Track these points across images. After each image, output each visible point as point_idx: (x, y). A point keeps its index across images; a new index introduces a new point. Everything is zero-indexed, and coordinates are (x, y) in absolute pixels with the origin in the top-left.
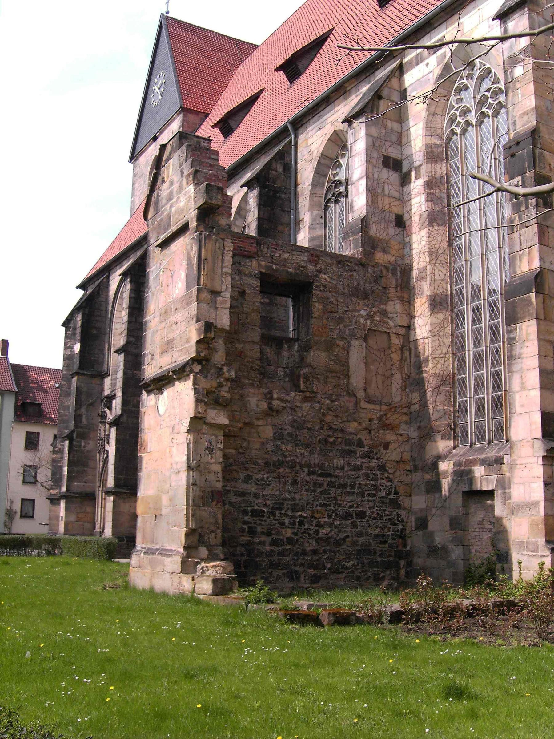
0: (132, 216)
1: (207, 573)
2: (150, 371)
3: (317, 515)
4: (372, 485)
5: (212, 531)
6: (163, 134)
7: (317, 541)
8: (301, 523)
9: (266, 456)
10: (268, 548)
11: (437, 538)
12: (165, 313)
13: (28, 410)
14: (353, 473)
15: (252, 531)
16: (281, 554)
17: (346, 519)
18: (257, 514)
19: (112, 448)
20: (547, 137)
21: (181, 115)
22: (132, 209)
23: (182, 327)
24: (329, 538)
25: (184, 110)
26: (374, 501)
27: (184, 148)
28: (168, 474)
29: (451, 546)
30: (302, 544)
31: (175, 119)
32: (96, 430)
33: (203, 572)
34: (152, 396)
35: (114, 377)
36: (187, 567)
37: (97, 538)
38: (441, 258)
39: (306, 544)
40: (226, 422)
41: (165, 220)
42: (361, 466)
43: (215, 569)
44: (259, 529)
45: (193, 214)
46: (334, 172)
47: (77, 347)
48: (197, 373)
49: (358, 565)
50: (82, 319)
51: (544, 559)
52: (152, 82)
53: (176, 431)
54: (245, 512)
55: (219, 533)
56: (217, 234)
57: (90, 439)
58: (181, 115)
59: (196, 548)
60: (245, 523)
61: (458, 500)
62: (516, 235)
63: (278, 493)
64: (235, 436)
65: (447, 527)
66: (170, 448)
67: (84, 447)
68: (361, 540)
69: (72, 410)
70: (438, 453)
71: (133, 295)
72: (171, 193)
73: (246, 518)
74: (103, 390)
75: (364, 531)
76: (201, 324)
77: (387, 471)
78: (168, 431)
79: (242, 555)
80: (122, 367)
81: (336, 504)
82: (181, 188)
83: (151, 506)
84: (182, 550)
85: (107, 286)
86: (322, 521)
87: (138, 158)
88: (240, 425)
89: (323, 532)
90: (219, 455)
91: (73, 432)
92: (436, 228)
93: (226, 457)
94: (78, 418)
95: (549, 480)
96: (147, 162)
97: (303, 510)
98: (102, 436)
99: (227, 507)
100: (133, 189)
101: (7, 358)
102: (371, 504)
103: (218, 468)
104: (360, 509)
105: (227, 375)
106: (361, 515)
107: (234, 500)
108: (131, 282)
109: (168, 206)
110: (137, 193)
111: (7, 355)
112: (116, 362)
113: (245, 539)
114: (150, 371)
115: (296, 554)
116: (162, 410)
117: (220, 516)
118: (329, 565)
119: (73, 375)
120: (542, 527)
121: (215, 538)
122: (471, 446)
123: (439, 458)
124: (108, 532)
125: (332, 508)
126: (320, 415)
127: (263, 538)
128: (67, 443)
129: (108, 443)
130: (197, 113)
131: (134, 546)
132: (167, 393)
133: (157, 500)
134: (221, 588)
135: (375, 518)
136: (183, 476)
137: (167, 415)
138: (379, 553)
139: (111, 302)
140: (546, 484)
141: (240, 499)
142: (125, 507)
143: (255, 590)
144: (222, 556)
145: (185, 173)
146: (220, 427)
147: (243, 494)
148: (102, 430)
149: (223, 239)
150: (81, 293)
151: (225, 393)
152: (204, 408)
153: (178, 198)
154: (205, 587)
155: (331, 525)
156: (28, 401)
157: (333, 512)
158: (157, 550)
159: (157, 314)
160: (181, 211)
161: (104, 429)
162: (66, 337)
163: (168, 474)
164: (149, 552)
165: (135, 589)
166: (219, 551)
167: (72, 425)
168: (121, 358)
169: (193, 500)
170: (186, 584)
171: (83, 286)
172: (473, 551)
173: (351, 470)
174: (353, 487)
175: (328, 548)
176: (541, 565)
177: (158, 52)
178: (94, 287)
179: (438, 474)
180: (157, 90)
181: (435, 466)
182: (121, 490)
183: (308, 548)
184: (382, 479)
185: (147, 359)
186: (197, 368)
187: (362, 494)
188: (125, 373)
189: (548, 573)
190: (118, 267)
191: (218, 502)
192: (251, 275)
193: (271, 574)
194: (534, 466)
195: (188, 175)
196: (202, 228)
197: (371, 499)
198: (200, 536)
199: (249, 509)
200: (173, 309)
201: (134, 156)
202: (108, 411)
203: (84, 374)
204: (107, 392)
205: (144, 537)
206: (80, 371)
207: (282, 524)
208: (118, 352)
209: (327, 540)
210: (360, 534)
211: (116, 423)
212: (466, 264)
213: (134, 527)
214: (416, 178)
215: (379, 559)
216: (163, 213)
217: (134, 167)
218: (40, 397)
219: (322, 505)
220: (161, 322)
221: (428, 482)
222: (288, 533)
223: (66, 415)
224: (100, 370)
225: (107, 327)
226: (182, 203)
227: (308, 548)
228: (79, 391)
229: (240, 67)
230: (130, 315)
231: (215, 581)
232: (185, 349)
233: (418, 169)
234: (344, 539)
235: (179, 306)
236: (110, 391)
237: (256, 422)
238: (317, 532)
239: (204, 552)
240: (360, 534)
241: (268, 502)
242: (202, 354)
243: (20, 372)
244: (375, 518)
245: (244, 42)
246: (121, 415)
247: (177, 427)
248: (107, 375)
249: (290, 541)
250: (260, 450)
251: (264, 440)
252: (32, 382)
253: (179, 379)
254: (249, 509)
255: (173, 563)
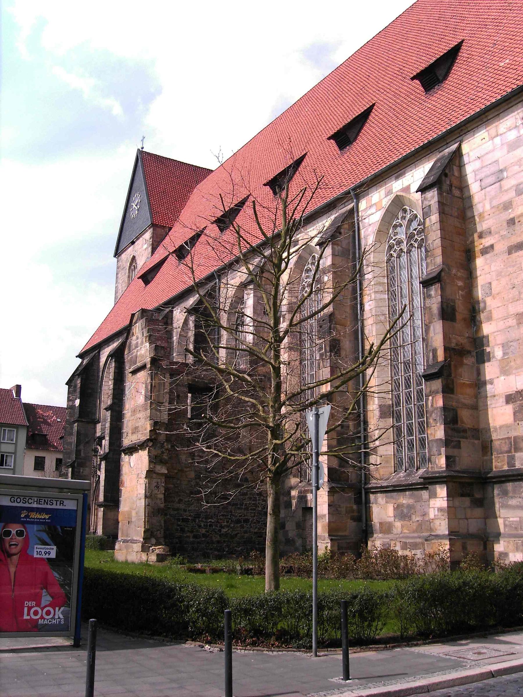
0: (115, 304)
1: (155, 552)
2: (127, 442)
3: (220, 521)
4: (253, 504)
5: (158, 530)
6: (139, 240)
7: (220, 536)
8: (211, 526)
9: (192, 489)
10: (191, 539)
11: (290, 534)
12: (134, 411)
13: (37, 440)
14: (242, 497)
15: (182, 530)
16: (198, 543)
17: (237, 523)
18: (185, 520)
19: (102, 474)
20: (339, 317)
21: (152, 229)
22: (116, 298)
23: (143, 420)
24: (227, 534)
25: (153, 225)
26: (254, 513)
27: (144, 319)
28: (135, 499)
29: (296, 539)
30: (211, 537)
31: (147, 231)
32: (91, 460)
33: (153, 552)
34: (127, 456)
35: (104, 423)
36: (144, 549)
37: (92, 536)
38: (295, 371)
39: (214, 538)
40: (166, 472)
41: (134, 358)
42: (247, 493)
43: (159, 549)
44: (186, 529)
45: (149, 359)
46: (242, 307)
47: (77, 402)
48: (150, 447)
49: (244, 549)
50: (81, 382)
51: (327, 544)
52: (131, 199)
53: (139, 477)
54: (178, 520)
55: (162, 532)
56: (161, 372)
57: (86, 467)
58: (152, 229)
59: (149, 539)
60: (178, 525)
61: (300, 512)
62: (321, 371)
63: (197, 509)
64: (173, 478)
65: (295, 528)
66: (137, 485)
67: (82, 472)
68: (246, 535)
69: (74, 446)
70: (291, 485)
71: (116, 371)
72: (137, 343)
73: (179, 523)
74: (95, 432)
75: (248, 530)
76: (152, 422)
77: (262, 495)
78: (135, 476)
79: (177, 543)
80: (109, 420)
81: (231, 515)
82: (142, 343)
83: (126, 516)
84: (142, 540)
85: (99, 358)
86: (223, 524)
87: (120, 255)
88: (176, 471)
89: (224, 530)
90: (162, 490)
91: (74, 462)
92: (293, 353)
93: (166, 489)
94: (78, 452)
95: (332, 504)
96: (127, 259)
97: (212, 518)
98: (95, 465)
99: (168, 517)
100: (117, 278)
101: (20, 399)
102: (253, 515)
103: (162, 496)
104: (246, 517)
105: (166, 447)
106: (246, 521)
107: (172, 513)
108: (115, 361)
109: (135, 351)
110: (120, 281)
111: (20, 396)
112: (106, 416)
113: (178, 534)
114: (127, 442)
115: (208, 543)
116: (132, 465)
117: (163, 522)
118: (227, 550)
119: (74, 422)
120: (327, 528)
121: (160, 534)
122: (308, 481)
123: (292, 488)
124: (100, 532)
125: (229, 517)
126: (223, 464)
127: (188, 534)
128: (70, 469)
129: (99, 470)
130: (164, 227)
131: (117, 538)
132: (135, 456)
133: (129, 513)
134: (161, 558)
135: (255, 523)
136: (143, 501)
137: (135, 467)
138: (257, 543)
139: (101, 370)
140: (329, 505)
141: (176, 512)
142: (111, 515)
143: (176, 559)
144: (163, 543)
145: (145, 335)
146: (162, 474)
147: (178, 509)
148: (95, 460)
149: (164, 374)
150: (79, 361)
151: (165, 457)
152: (154, 465)
153: (141, 348)
154: (153, 558)
155: (228, 526)
156: (36, 432)
157: (230, 519)
158: (129, 540)
159: (130, 411)
160: (142, 356)
161: (96, 461)
162: (69, 393)
163: (135, 499)
164: (125, 541)
165: (117, 562)
166: (162, 540)
167: (74, 456)
168: (108, 414)
169: (148, 514)
170: (144, 557)
171: (81, 356)
172: (308, 541)
173: (241, 495)
174: (242, 505)
175: (227, 540)
176: (326, 547)
177: (136, 177)
178: (90, 354)
179: (290, 497)
180: (134, 206)
181: (289, 493)
182: (108, 504)
183: (215, 539)
184: (259, 500)
185: (124, 435)
186: (150, 444)
187: (247, 509)
188: (111, 424)
189: (329, 551)
190: (106, 346)
191: (162, 515)
192: (183, 386)
193: (193, 554)
194: (325, 496)
195: (146, 337)
196: (153, 368)
197: (252, 511)
198: (152, 532)
199: (181, 518)
200: (138, 410)
201: (118, 253)
202: (99, 448)
203: (82, 421)
204: (98, 434)
205: (122, 533)
206: (80, 419)
207: (200, 526)
208: (107, 409)
209: (226, 535)
210: (246, 532)
211: (105, 458)
212: (308, 376)
213: (117, 528)
214: (283, 322)
215: (257, 546)
216: (132, 354)
217: (118, 261)
218: (45, 430)
219: (223, 515)
220: (132, 416)
221: (286, 502)
222: (204, 531)
223: (69, 449)
224: (93, 418)
225: (99, 388)
226: (143, 351)
227: (215, 539)
228: (78, 433)
229: (195, 190)
230: (115, 384)
231: (158, 555)
232: (143, 435)
233: (284, 318)
234: (236, 535)
235: (141, 409)
236: (100, 433)
237: (185, 469)
238: (220, 530)
239: (153, 541)
240: (246, 532)
241: (192, 514)
242: (153, 437)
243: (30, 409)
244: (255, 523)
245: (199, 167)
246: (108, 453)
247: (140, 475)
248: (99, 422)
249: (204, 535)
250: (187, 485)
251: (190, 480)
252: (39, 418)
253: (141, 449)
254: (181, 518)
255: (137, 547)
